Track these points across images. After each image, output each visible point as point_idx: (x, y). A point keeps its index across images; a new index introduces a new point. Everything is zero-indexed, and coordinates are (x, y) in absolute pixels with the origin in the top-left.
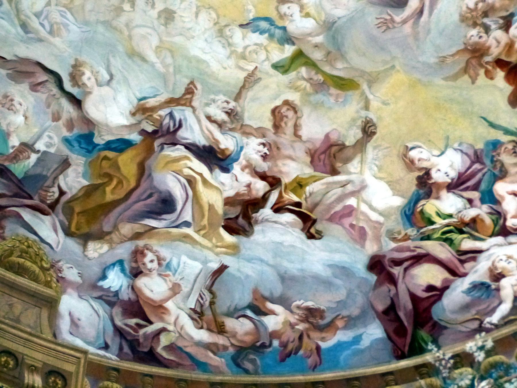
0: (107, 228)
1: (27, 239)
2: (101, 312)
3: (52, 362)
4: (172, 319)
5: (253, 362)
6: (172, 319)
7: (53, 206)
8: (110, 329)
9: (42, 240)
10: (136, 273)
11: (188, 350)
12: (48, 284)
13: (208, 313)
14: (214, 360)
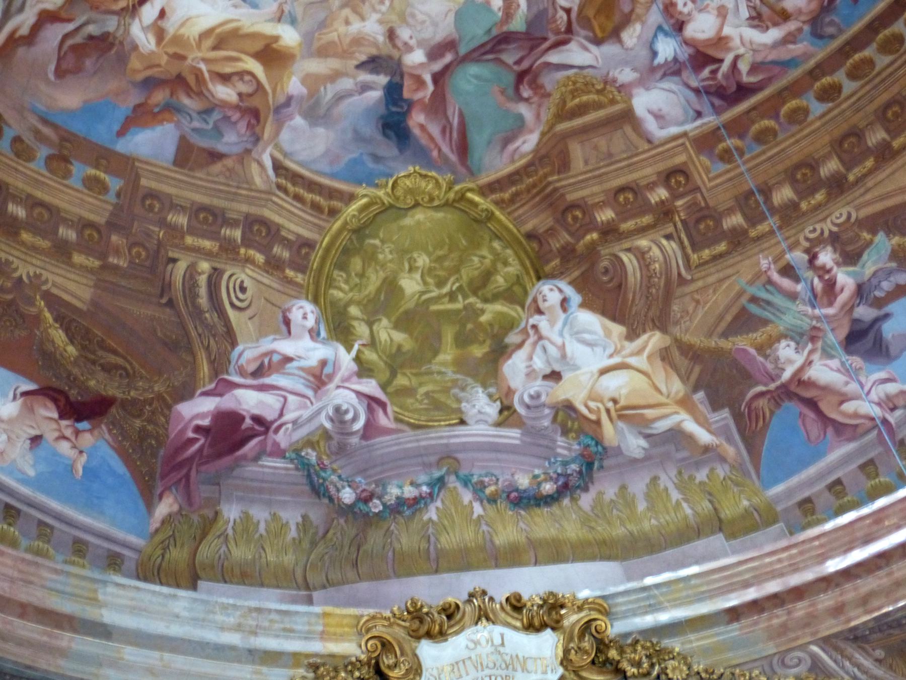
0: (626, 9)
1: (568, 78)
2: (674, 87)
3: (662, 166)
4: (737, 42)
5: (832, 23)
6: (737, 42)
7: (569, 30)
8: (691, 95)
9: (581, 68)
10: (680, 26)
11: (771, 57)
12: (613, 102)
13: (765, 11)
14: (797, 49)
